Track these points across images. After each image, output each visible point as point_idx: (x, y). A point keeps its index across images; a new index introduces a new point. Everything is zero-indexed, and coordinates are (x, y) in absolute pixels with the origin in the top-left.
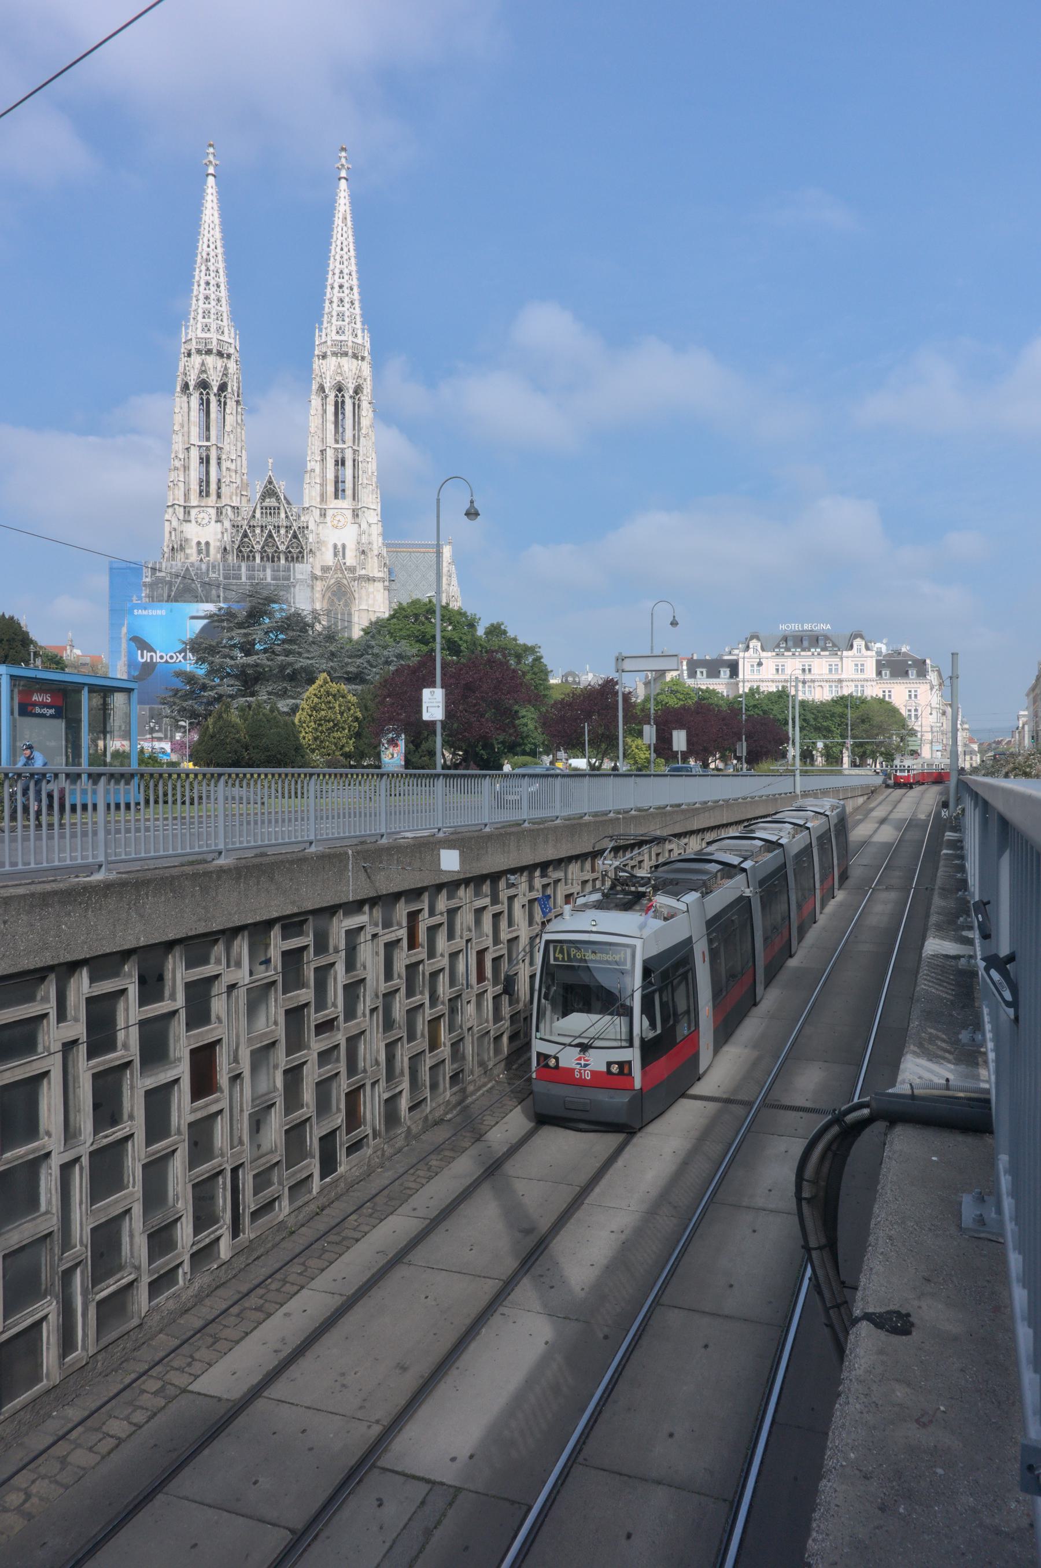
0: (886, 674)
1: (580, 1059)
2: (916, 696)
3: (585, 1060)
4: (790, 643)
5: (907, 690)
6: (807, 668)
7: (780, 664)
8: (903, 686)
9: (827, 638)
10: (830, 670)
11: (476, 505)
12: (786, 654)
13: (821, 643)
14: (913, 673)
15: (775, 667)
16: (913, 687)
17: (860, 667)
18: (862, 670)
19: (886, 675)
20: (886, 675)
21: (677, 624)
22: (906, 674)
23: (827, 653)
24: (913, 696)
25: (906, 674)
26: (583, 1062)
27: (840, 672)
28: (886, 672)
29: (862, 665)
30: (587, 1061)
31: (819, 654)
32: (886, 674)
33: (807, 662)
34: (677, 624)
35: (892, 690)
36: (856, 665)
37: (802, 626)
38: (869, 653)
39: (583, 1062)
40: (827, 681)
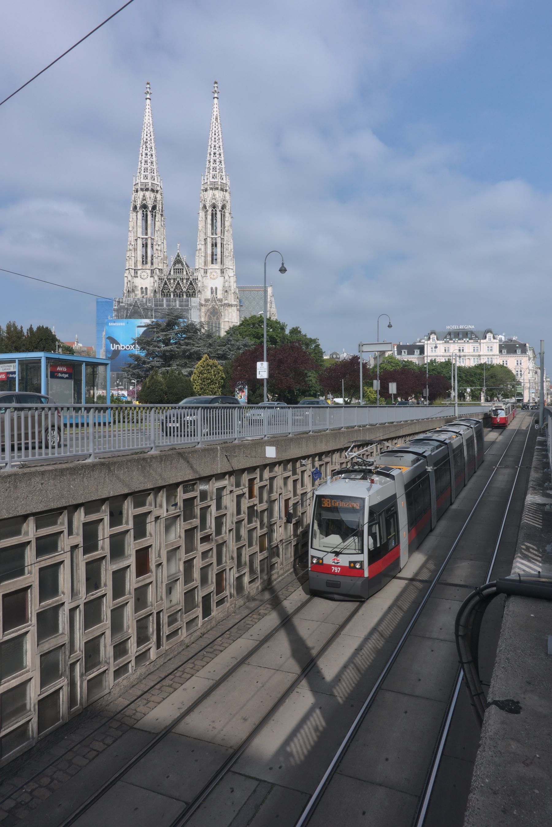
1: (334, 559)
2: (521, 363)
4: (452, 336)
5: (516, 360)
6: (461, 349)
7: (490, 346)
9: (472, 333)
10: (474, 350)
11: (285, 265)
12: (450, 341)
13: (469, 336)
14: (519, 351)
15: (444, 349)
16: (519, 359)
17: (490, 348)
18: (491, 350)
20: (504, 353)
22: (515, 352)
23: (472, 341)
24: (519, 364)
25: (515, 352)
26: (336, 561)
27: (479, 351)
28: (504, 351)
29: (491, 347)
30: (338, 560)
31: (468, 342)
33: (461, 346)
36: (488, 347)
37: (459, 327)
38: (495, 341)
39: (336, 561)
40: (486, 356)
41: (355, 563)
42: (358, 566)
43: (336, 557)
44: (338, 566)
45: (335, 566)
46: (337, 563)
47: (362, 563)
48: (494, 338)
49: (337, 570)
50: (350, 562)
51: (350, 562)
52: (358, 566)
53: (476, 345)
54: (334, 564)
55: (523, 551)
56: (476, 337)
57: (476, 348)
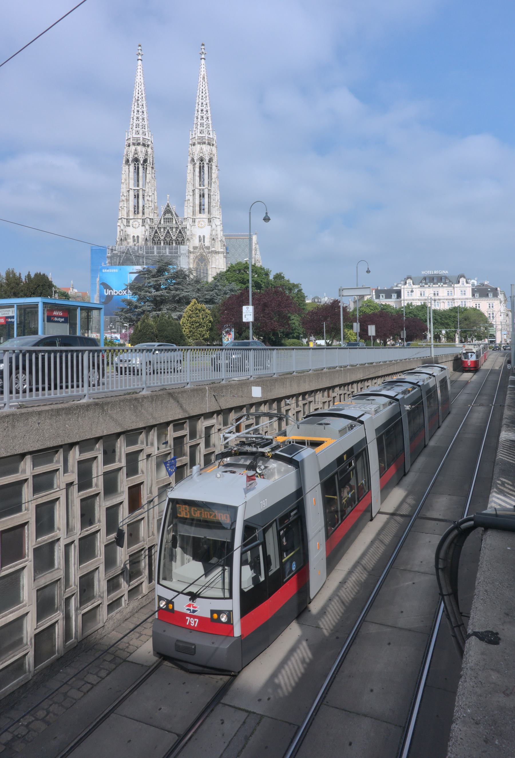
0: (477, 295)
1: (189, 605)
3: (194, 607)
4: (427, 281)
5: (488, 304)
6: (436, 293)
8: (486, 302)
9: (446, 278)
10: (448, 294)
12: (425, 286)
14: (491, 295)
15: (420, 293)
17: (463, 292)
19: (477, 296)
20: (477, 296)
21: (269, 219)
22: (487, 296)
23: (446, 285)
24: (491, 307)
28: (477, 295)
29: (465, 291)
30: (195, 607)
32: (477, 295)
33: (436, 290)
34: (269, 219)
35: (480, 304)
36: (462, 291)
37: (434, 272)
38: (468, 285)
39: (192, 609)
40: (460, 299)
41: (219, 612)
42: (224, 619)
43: (191, 602)
44: (195, 617)
45: (191, 616)
46: (194, 611)
47: (230, 614)
48: (467, 283)
49: (193, 622)
50: (213, 612)
51: (213, 612)
52: (224, 619)
53: (450, 289)
54: (188, 612)
55: (498, 486)
56: (450, 281)
57: (450, 292)
